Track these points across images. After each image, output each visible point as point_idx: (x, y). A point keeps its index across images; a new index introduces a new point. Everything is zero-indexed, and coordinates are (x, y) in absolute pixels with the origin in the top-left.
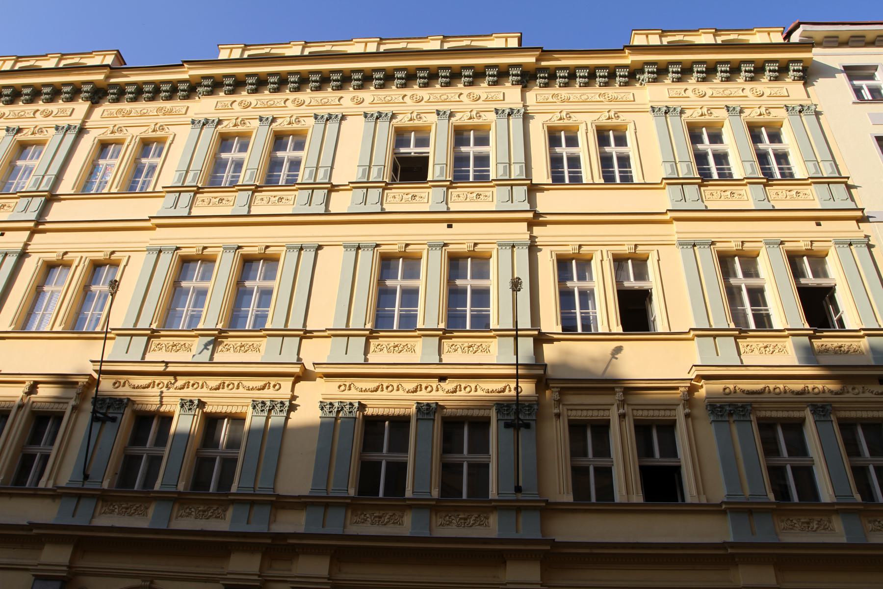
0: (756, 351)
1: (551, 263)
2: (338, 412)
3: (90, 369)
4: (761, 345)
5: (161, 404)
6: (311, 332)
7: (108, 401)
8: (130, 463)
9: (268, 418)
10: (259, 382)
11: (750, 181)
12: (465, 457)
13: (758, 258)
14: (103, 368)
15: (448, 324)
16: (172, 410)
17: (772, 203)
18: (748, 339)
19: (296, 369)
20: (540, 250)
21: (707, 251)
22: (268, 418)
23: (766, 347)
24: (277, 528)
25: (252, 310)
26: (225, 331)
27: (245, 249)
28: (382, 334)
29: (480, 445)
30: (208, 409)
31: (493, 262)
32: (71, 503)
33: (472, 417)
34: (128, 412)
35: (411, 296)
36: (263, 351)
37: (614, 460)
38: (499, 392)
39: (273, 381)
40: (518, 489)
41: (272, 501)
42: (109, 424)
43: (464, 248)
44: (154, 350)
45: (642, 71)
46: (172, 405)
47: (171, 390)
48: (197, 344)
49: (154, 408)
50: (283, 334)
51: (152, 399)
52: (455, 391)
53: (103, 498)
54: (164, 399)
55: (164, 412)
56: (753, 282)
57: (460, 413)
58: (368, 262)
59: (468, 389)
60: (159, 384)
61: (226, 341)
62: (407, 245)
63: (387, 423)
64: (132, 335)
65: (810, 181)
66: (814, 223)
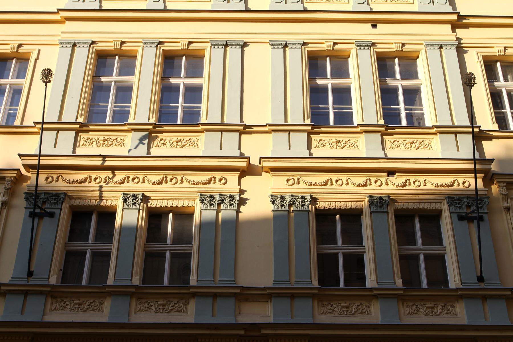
1: (479, 64)
2: (290, 205)
3: (18, 163)
5: (101, 198)
6: (251, 127)
7: (43, 196)
8: (72, 260)
9: (218, 212)
10: (204, 177)
12: (340, 248)
13: (349, 59)
14: (42, 162)
15: (160, 119)
16: (113, 204)
18: (395, 136)
19: (243, 163)
20: (466, 52)
21: (297, 52)
22: (218, 212)
23: (412, 143)
25: (110, 105)
26: (86, 125)
27: (100, 44)
28: (166, 128)
29: (434, 236)
30: (152, 203)
31: (352, 63)
32: (286, 303)
33: (424, 210)
34: (65, 207)
35: (125, 92)
36: (202, 145)
37: (366, 247)
38: (448, 186)
39: (218, 175)
40: (481, 279)
41: (235, 293)
42: (46, 219)
43: (393, 48)
44: (84, 145)
46: (113, 198)
47: (110, 185)
48: (130, 140)
49: (93, 202)
50: (221, 128)
51: (90, 194)
52: (405, 186)
53: (52, 293)
54: (104, 194)
55: (105, 207)
56: (410, 82)
57: (411, 206)
58: (297, 60)
59: (417, 183)
60: (95, 179)
61: (161, 136)
62: (190, 43)
63: (338, 217)
64: (58, 130)
66: (370, 25)
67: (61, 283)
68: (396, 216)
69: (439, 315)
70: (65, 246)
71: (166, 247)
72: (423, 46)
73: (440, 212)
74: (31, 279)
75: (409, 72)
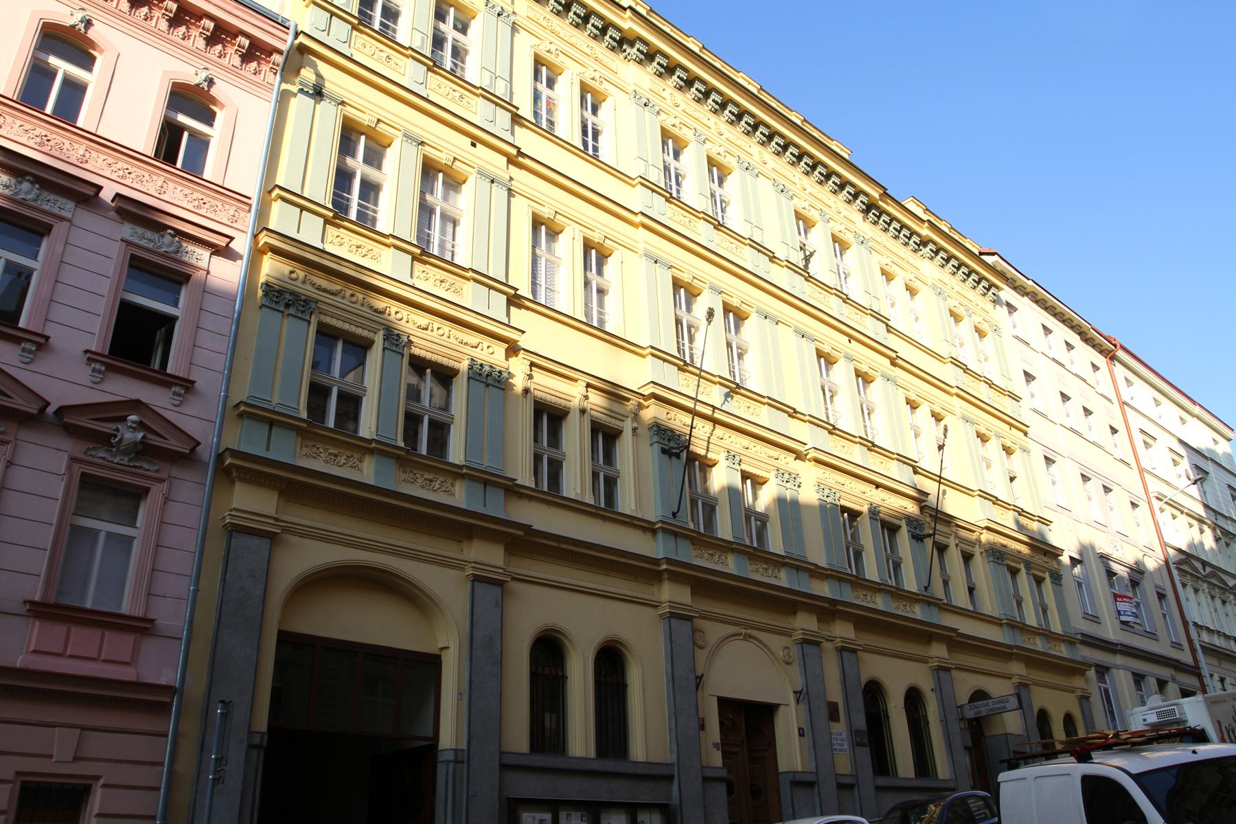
0: (431, 281)
4: (438, 277)
11: (414, 54)
17: (352, 51)
23: (358, 247)
45: (632, 45)
56: (372, 173)
65: (410, 52)
66: (469, 141)
68: (318, 332)
72: (399, 134)
73: (900, 527)
75: (374, 158)
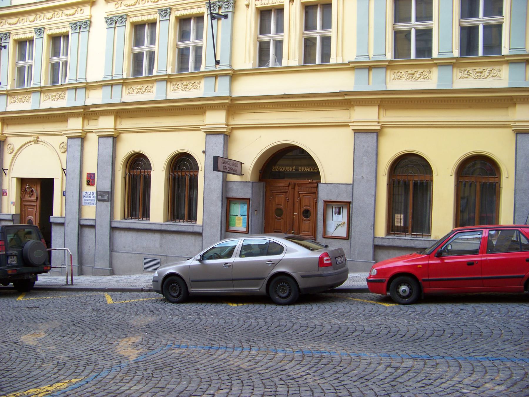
24: (88, 102)
34: (11, 41)
40: (217, 63)
53: (124, 83)
67: (259, 66)
69: (486, 78)
70: (303, 34)
71: (270, 37)
74: (218, 66)
